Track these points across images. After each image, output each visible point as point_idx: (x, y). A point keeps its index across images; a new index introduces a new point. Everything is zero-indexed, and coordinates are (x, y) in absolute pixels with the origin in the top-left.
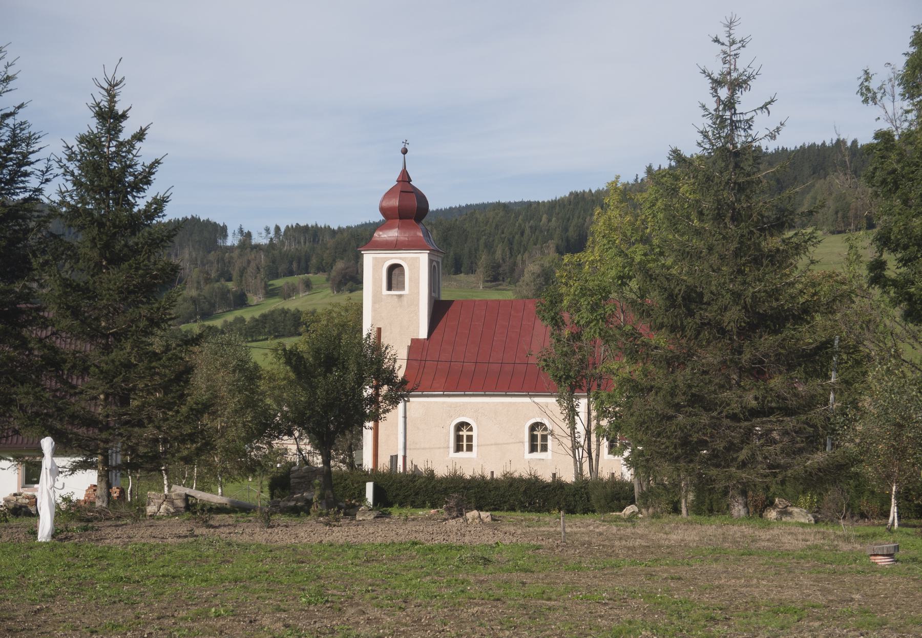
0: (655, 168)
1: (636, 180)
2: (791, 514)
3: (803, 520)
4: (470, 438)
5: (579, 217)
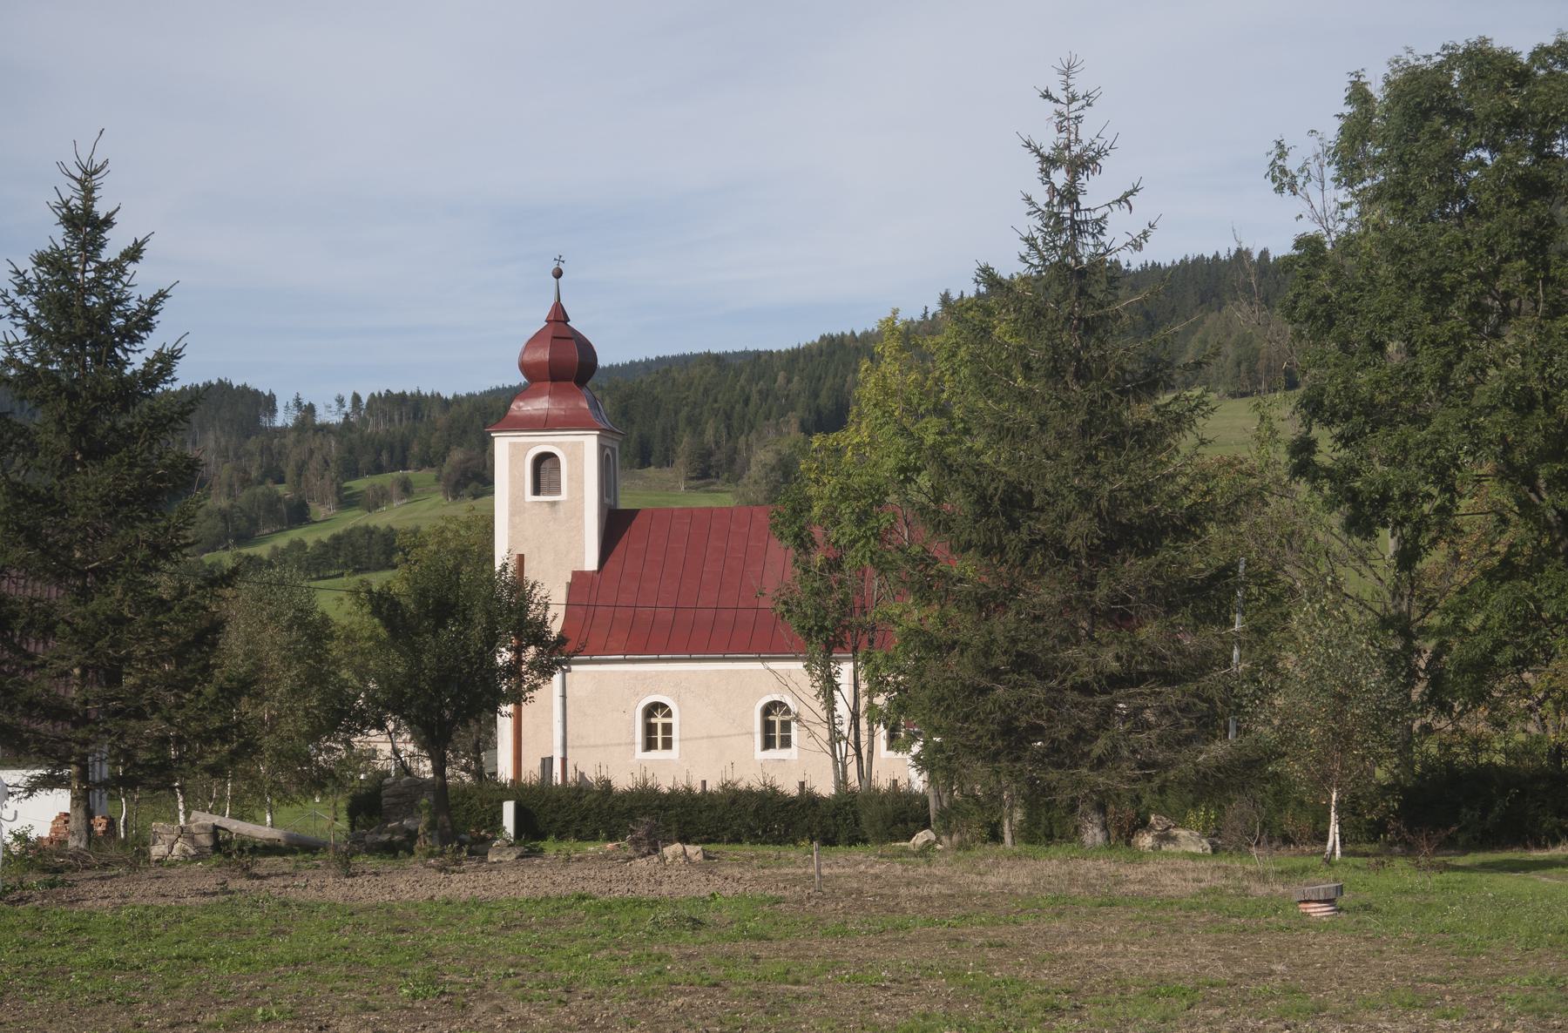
0: (955, 296)
1: (925, 316)
2: (1174, 839)
3: (1193, 849)
4: (667, 728)
5: (835, 376)
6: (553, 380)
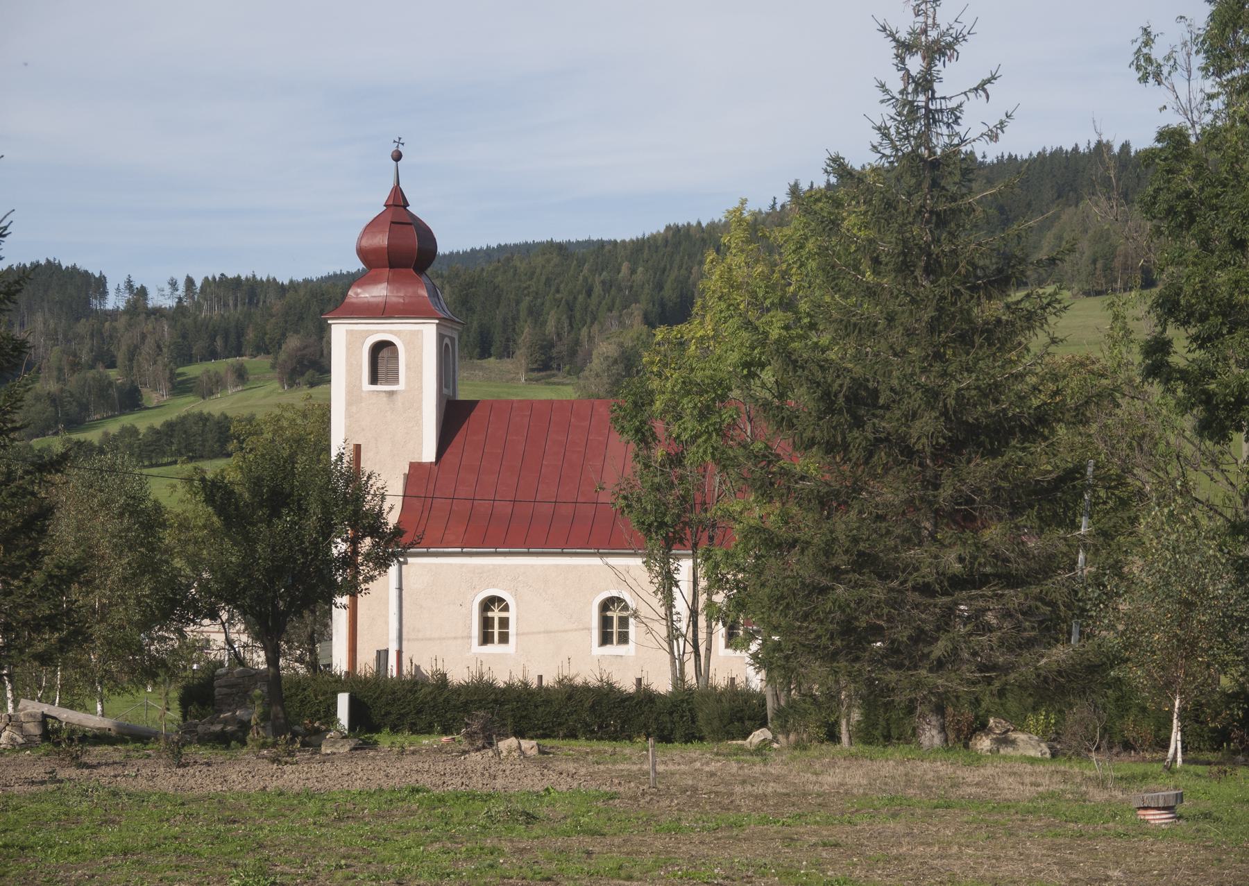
0: (805, 186)
1: (773, 207)
2: (1013, 742)
4: (504, 623)
5: (680, 268)
6: (391, 267)
